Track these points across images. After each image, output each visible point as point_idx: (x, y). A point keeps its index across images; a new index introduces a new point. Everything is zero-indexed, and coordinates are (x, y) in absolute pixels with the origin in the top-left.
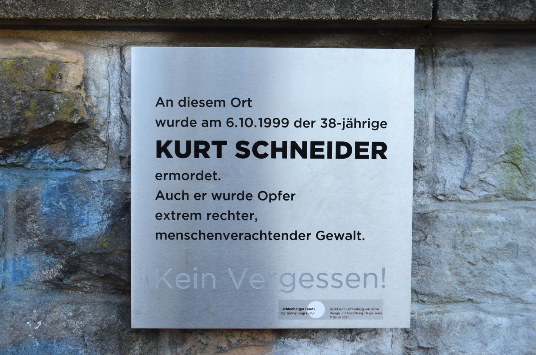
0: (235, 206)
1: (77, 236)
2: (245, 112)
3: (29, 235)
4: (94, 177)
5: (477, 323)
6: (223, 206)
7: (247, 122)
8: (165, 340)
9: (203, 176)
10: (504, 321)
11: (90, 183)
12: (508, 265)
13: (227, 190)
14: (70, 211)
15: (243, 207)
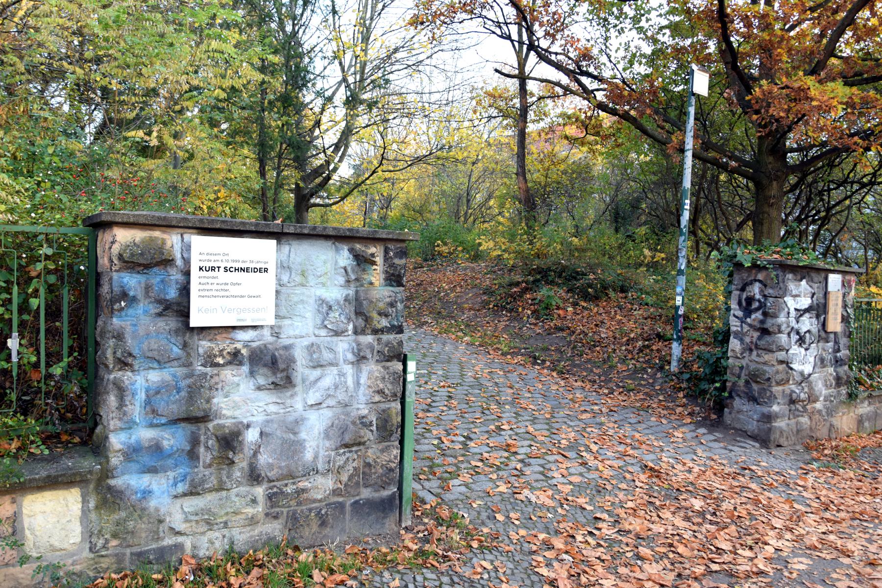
0: (223, 287)
1: (168, 297)
2: (226, 258)
3: (150, 297)
4: (172, 278)
5: (292, 325)
6: (219, 287)
7: (227, 261)
8: (196, 331)
9: (213, 278)
10: (300, 324)
11: (171, 280)
12: (301, 306)
13: (221, 282)
14: (164, 289)
15: (226, 287)
